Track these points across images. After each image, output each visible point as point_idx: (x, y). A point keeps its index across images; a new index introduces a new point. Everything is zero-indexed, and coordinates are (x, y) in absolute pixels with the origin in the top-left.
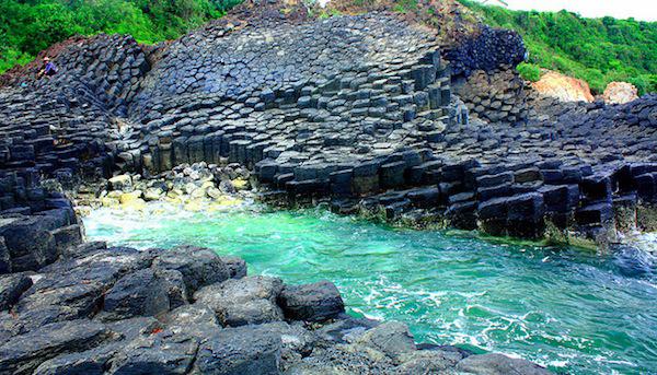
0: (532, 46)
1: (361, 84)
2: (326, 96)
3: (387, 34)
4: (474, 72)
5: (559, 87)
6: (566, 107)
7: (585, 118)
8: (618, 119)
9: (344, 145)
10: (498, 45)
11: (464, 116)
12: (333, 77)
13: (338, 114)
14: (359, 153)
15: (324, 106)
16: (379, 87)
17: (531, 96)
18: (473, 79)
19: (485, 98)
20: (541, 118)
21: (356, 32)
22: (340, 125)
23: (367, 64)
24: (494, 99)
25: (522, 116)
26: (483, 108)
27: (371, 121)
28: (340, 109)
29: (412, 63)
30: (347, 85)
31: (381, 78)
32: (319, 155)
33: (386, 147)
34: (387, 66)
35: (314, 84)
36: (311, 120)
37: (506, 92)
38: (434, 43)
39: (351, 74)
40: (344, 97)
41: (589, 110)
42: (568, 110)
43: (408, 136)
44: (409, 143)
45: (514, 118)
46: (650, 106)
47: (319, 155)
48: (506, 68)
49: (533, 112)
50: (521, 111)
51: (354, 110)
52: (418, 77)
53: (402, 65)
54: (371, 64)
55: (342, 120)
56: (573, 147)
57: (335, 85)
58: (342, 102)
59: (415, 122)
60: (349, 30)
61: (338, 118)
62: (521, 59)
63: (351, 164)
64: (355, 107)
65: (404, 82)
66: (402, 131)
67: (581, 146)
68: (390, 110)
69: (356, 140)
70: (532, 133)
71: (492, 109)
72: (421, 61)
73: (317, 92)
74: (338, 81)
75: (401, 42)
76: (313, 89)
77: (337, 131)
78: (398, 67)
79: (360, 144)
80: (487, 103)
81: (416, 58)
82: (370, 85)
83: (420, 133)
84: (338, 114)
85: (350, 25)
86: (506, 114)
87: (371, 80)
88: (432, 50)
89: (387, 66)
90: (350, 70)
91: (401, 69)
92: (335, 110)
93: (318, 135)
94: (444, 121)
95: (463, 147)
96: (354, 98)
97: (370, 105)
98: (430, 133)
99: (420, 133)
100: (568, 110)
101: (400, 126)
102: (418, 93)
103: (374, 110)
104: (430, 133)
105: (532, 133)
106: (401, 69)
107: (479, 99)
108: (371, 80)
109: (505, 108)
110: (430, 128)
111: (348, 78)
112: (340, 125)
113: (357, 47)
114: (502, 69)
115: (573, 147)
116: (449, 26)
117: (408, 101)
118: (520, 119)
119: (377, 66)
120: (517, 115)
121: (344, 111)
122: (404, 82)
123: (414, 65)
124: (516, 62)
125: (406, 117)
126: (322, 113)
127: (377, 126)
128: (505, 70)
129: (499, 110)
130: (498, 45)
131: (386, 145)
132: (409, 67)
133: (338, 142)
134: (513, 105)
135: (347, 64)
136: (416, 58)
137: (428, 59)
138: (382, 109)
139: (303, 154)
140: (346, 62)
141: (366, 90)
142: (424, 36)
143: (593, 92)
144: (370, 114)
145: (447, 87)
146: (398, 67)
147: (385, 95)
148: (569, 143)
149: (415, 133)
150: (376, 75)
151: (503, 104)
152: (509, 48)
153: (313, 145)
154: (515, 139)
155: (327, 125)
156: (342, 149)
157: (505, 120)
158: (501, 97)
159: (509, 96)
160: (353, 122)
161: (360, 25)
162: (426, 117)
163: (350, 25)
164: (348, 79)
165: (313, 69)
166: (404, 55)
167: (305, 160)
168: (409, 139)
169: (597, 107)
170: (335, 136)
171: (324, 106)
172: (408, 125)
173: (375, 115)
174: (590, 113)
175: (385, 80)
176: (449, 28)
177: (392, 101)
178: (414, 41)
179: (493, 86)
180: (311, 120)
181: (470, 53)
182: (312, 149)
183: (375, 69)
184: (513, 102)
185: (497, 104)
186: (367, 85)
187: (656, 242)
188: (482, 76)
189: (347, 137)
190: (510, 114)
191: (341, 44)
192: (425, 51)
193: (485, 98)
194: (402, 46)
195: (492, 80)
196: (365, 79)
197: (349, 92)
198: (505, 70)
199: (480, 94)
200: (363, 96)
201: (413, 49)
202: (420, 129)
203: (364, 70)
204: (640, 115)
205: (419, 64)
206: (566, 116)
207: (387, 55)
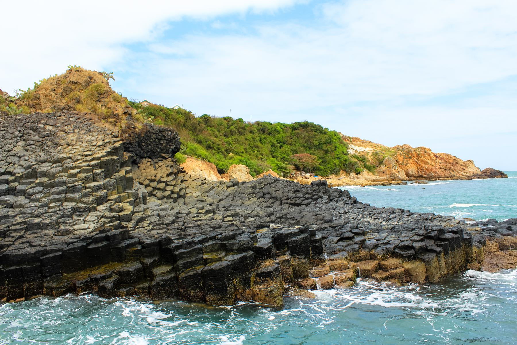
0: (184, 137)
1: (57, 173)
2: (24, 184)
3: (76, 131)
4: (144, 160)
5: (197, 168)
6: (212, 185)
7: (227, 193)
8: (250, 194)
9: (46, 229)
10: (160, 140)
11: (144, 198)
12: (29, 167)
13: (38, 200)
14: (62, 235)
15: (23, 193)
16: (74, 175)
17: (185, 178)
18: (142, 166)
19: (152, 181)
20: (195, 195)
21: (49, 128)
22: (40, 211)
23: (62, 155)
24: (160, 182)
25: (182, 193)
26: (152, 189)
27: (68, 205)
28: (39, 196)
29: (100, 155)
30: (44, 174)
31: (76, 167)
32: (24, 240)
33: (87, 225)
34: (79, 157)
35: (11, 173)
36: (12, 206)
37: (168, 175)
38: (118, 139)
39: (47, 164)
40: (41, 184)
41: (228, 187)
42: (213, 188)
43: (103, 217)
44: (105, 223)
45: (176, 196)
46: (270, 184)
47: (24, 240)
48: (167, 157)
49: (188, 190)
50: (180, 190)
51: (52, 197)
52: (108, 168)
53: (91, 157)
54: (65, 156)
55: (42, 206)
56: (231, 219)
57: (33, 174)
58: (40, 189)
59: (108, 204)
60: (42, 126)
61: (37, 204)
62: (177, 150)
63: (59, 247)
64: (53, 194)
65: (95, 171)
66: (97, 214)
67: (238, 218)
68: (86, 195)
69: (58, 223)
70: (199, 209)
71: (159, 189)
72: (109, 154)
73: (14, 181)
74: (35, 171)
75: (89, 138)
76: (11, 178)
77: (38, 216)
78: (89, 158)
79: (62, 227)
80: (154, 184)
81: (104, 151)
82: (66, 174)
83: (113, 214)
84: (38, 200)
85: (43, 121)
86: (169, 193)
87: (66, 170)
88: (117, 145)
89: (79, 157)
90: (45, 161)
91: (93, 160)
92: (34, 197)
93: (20, 220)
94: (130, 203)
95: (149, 224)
96: (52, 186)
97: (66, 192)
98: (122, 214)
99: (113, 214)
100: (213, 188)
101: (95, 209)
102: (107, 180)
103: (70, 195)
104: (122, 214)
105: (199, 209)
106: (93, 160)
107: (148, 182)
108: (66, 170)
109: (168, 188)
110: (122, 210)
111: (45, 167)
112: (40, 211)
113: (51, 140)
114: (164, 158)
115: (231, 219)
116: (123, 124)
117: (99, 188)
118: (179, 196)
119: (70, 158)
120: (178, 193)
121: (43, 197)
122: (95, 171)
123: (103, 157)
124: (174, 152)
125: (100, 201)
126: (21, 200)
127: (75, 210)
128: (166, 159)
129: (164, 190)
130: (160, 140)
131: (86, 226)
132: (99, 159)
133: (40, 226)
134: (174, 186)
135: (42, 156)
136: (104, 151)
137: (114, 151)
138: (77, 195)
139: (6, 239)
140: (41, 154)
141: (62, 179)
142: (108, 132)
143: (221, 172)
144: (66, 200)
145: (130, 175)
146: (89, 158)
147: (79, 183)
148: (229, 216)
149: (108, 214)
150: (71, 165)
151: (167, 185)
152: (169, 141)
153: (15, 230)
154: (187, 214)
155: (28, 210)
156: (46, 232)
157: (169, 197)
158: (164, 179)
159: (171, 178)
160: (53, 207)
161: (51, 122)
162: (115, 200)
163: (43, 121)
164: (44, 169)
165: (10, 159)
166: (93, 148)
167: (10, 245)
168: (103, 220)
169: (234, 185)
170: (37, 220)
171: (23, 193)
172: (100, 208)
173: (72, 200)
174: (229, 189)
175: (79, 170)
176: (123, 126)
177: (86, 188)
178: (101, 137)
179: (161, 170)
180: (12, 206)
181: (140, 145)
182: (15, 234)
183: (69, 160)
184: (173, 184)
185: (162, 185)
186: (63, 174)
187: (514, 252)
188: (149, 164)
189: (48, 221)
190: (172, 192)
191: (36, 138)
192: (111, 146)
193: (152, 181)
194: (90, 142)
195: (157, 166)
196: (59, 169)
197: (45, 180)
198: (166, 159)
199: (149, 178)
200: (59, 184)
201: (100, 143)
202: (111, 210)
203: (59, 161)
204: (265, 190)
205: (106, 156)
206: (212, 193)
207: (78, 149)
